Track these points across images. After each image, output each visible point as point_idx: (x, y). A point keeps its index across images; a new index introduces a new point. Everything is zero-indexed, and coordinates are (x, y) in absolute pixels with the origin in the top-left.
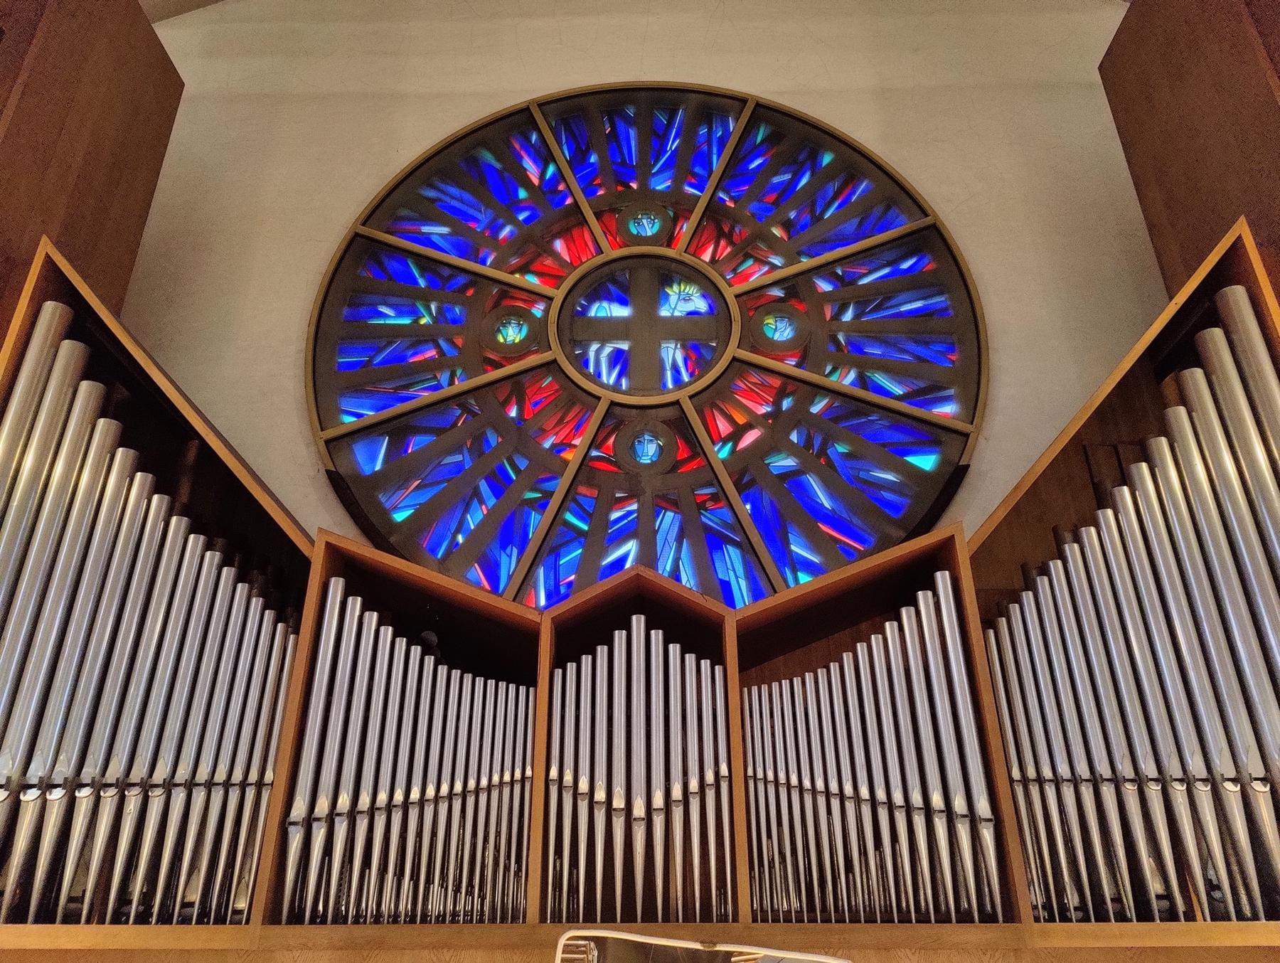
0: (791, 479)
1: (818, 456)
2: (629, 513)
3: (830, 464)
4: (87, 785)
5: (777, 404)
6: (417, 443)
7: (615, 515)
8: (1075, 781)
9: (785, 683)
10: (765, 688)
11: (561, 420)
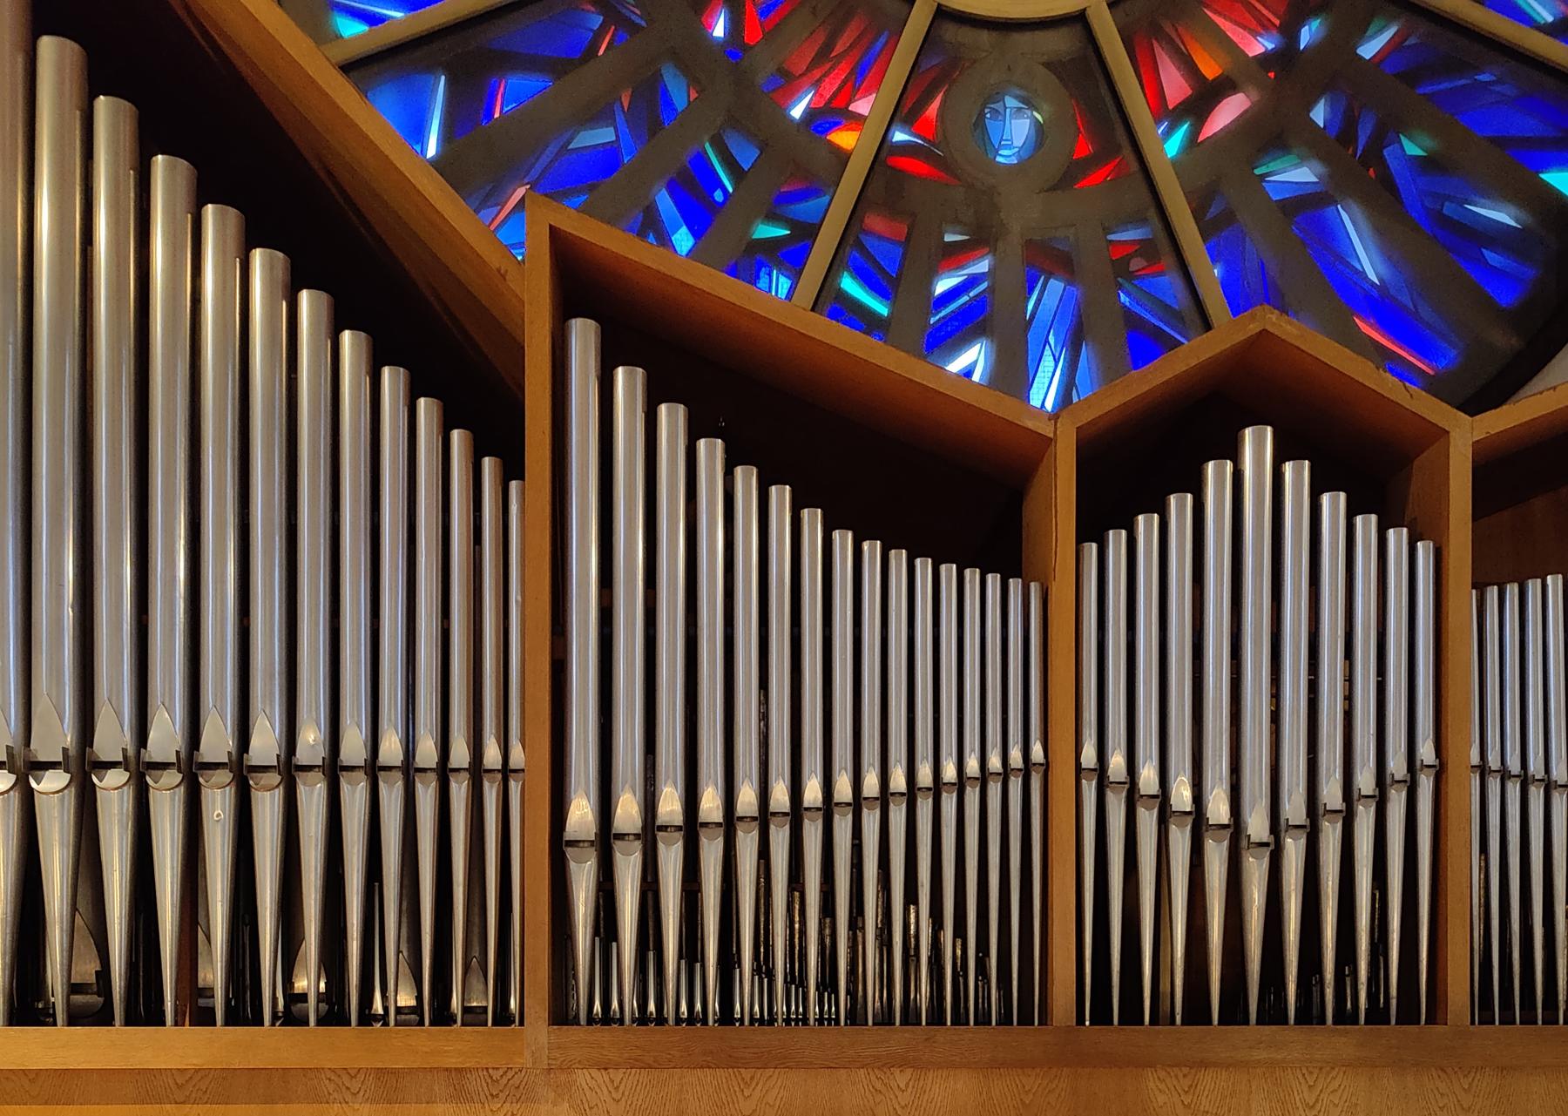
0: (1307, 211)
1: (1365, 162)
2: (972, 281)
3: (1387, 183)
4: (52, 765)
5: (1289, 32)
6: (513, 94)
7: (943, 285)
8: (1505, 775)
9: (1512, 590)
10: (1512, 590)
11: (828, 46)
